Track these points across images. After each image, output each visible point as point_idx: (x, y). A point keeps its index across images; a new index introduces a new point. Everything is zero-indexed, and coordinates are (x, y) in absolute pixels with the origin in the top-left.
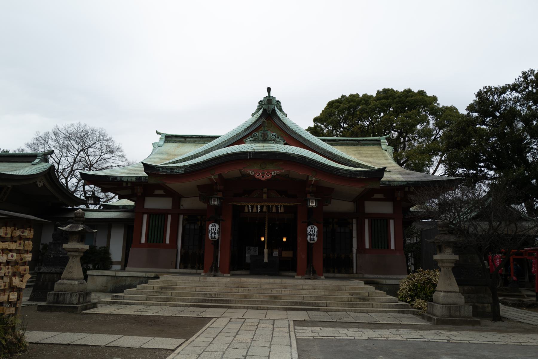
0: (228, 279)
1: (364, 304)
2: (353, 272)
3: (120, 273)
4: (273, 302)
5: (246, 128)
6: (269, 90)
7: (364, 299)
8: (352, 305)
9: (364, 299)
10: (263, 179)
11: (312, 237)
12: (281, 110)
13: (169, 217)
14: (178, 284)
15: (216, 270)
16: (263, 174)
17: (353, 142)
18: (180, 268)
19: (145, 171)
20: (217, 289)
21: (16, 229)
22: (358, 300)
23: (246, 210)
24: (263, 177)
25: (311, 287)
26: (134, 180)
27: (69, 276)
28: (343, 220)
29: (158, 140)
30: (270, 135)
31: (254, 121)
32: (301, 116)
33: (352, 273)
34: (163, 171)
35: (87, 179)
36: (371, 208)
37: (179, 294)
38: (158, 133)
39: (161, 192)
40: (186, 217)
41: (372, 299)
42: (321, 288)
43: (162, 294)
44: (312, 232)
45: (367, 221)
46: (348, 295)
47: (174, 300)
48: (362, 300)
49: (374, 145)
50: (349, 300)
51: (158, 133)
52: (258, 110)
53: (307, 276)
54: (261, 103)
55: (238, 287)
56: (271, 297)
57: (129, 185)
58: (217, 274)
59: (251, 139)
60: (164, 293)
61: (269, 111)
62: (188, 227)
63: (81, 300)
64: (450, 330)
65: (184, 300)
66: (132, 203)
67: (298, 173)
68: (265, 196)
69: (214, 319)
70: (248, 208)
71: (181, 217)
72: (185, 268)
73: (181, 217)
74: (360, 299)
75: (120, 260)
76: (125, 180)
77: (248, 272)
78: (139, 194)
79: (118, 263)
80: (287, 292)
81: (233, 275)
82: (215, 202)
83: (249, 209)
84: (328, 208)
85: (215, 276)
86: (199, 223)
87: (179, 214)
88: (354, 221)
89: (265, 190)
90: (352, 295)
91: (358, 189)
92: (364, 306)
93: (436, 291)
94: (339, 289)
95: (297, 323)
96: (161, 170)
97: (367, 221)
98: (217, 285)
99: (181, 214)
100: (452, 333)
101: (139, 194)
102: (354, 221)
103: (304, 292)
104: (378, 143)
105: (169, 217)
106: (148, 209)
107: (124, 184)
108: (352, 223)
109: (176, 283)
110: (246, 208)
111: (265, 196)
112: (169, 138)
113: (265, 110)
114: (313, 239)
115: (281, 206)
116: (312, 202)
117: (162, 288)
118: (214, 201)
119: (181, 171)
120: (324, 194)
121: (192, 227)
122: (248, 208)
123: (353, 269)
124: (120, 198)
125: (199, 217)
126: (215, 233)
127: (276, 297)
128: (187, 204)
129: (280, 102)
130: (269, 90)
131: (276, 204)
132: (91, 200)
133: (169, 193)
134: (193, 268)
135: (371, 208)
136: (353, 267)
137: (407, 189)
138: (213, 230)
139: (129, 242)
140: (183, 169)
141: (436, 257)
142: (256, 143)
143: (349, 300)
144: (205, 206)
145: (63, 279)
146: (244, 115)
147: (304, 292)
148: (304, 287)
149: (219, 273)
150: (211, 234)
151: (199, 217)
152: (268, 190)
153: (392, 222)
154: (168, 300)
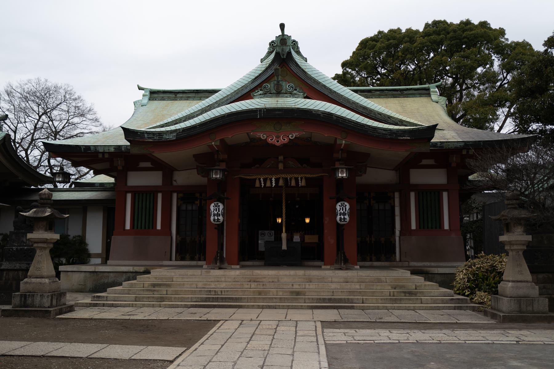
0: (238, 272)
1: (410, 299)
2: (395, 259)
3: (101, 267)
4: (294, 299)
5: (253, 78)
6: (282, 26)
7: (410, 293)
8: (395, 301)
9: (410, 293)
10: (278, 144)
11: (342, 217)
12: (298, 53)
13: (160, 196)
14: (174, 280)
15: (222, 260)
16: (278, 137)
17: (394, 92)
18: (176, 260)
19: (126, 138)
20: (223, 285)
21: (374, 258)
22: (403, 294)
23: (257, 185)
24: (278, 141)
25: (342, 280)
26: (112, 150)
27: (38, 273)
28: (382, 193)
29: (140, 98)
30: (286, 86)
31: (263, 69)
32: (325, 60)
33: (395, 260)
34: (149, 138)
35: (53, 150)
36: (418, 177)
37: (176, 292)
38: (140, 88)
39: (148, 164)
40: (181, 195)
41: (420, 292)
42: (356, 280)
43: (155, 293)
44: (343, 210)
45: (412, 195)
46: (390, 288)
47: (170, 300)
48: (407, 295)
49: (421, 95)
50: (392, 294)
51: (140, 88)
52: (269, 53)
53: (337, 266)
54: (272, 44)
55: (250, 282)
56: (292, 293)
57: (107, 156)
58: (223, 266)
59: (261, 92)
60: (158, 291)
61: (283, 55)
62: (184, 207)
63: (54, 302)
64: (520, 329)
65: (182, 300)
66: (112, 180)
67: (323, 135)
68: (281, 166)
69: (221, 322)
70: (260, 183)
71: (175, 196)
72: (183, 259)
73: (175, 196)
74: (405, 292)
75: (100, 251)
76: (101, 150)
77: (262, 263)
78: (120, 168)
79: (97, 256)
80: (312, 286)
81: (243, 267)
82: (216, 176)
83: (260, 183)
84: (361, 179)
85: (220, 268)
86: (198, 202)
87: (172, 192)
88: (397, 195)
89: (281, 158)
90: (395, 289)
91: (402, 153)
92: (411, 302)
93: (502, 280)
94: (379, 281)
95: (326, 324)
96: (146, 136)
97: (412, 195)
98: (223, 279)
99: (129, 192)
100: (522, 332)
101: (120, 168)
102: (397, 195)
103: (333, 286)
104: (426, 93)
105: (160, 196)
106: (132, 187)
107: (100, 156)
108: (394, 198)
109: (171, 279)
110: (257, 181)
111: (281, 166)
112: (155, 95)
113: (277, 54)
114: (344, 219)
115: (301, 178)
116: (342, 172)
117: (154, 285)
118: (216, 174)
119: (172, 137)
120: (357, 161)
121: (190, 208)
122: (260, 181)
123: (395, 256)
124: (96, 173)
125: (198, 195)
126: (218, 215)
127: (298, 293)
128: (182, 178)
129: (297, 42)
130: (282, 26)
131: (296, 176)
132: (59, 176)
133: (158, 165)
134: (192, 259)
135: (418, 177)
136: (395, 253)
137: (464, 152)
138: (216, 211)
139: (111, 229)
140: (175, 134)
141: (502, 238)
142: (267, 97)
143: (392, 294)
144: (204, 180)
145: (30, 277)
146: (251, 62)
147: (333, 286)
148: (334, 280)
149: (226, 265)
150: (214, 215)
151: (198, 195)
152: (284, 158)
153: (445, 195)
154: (162, 299)
